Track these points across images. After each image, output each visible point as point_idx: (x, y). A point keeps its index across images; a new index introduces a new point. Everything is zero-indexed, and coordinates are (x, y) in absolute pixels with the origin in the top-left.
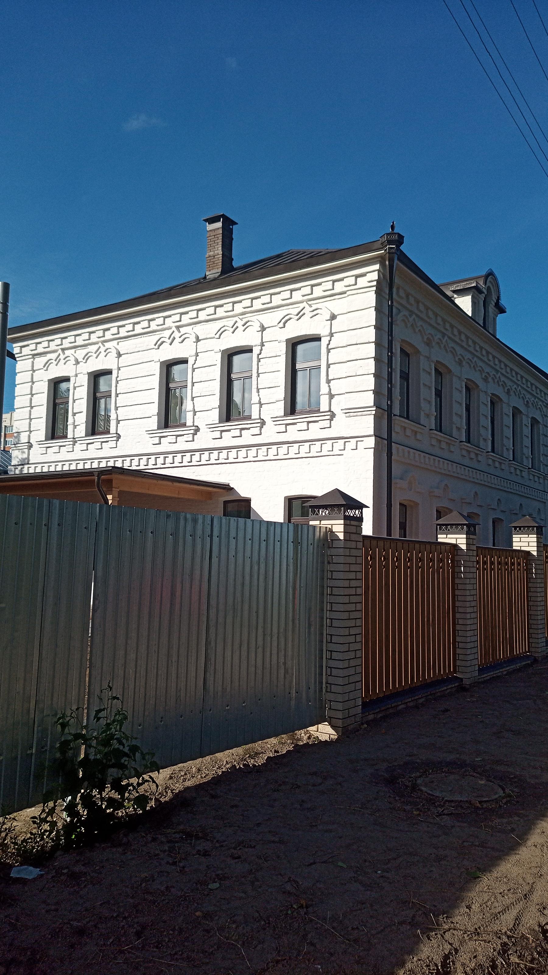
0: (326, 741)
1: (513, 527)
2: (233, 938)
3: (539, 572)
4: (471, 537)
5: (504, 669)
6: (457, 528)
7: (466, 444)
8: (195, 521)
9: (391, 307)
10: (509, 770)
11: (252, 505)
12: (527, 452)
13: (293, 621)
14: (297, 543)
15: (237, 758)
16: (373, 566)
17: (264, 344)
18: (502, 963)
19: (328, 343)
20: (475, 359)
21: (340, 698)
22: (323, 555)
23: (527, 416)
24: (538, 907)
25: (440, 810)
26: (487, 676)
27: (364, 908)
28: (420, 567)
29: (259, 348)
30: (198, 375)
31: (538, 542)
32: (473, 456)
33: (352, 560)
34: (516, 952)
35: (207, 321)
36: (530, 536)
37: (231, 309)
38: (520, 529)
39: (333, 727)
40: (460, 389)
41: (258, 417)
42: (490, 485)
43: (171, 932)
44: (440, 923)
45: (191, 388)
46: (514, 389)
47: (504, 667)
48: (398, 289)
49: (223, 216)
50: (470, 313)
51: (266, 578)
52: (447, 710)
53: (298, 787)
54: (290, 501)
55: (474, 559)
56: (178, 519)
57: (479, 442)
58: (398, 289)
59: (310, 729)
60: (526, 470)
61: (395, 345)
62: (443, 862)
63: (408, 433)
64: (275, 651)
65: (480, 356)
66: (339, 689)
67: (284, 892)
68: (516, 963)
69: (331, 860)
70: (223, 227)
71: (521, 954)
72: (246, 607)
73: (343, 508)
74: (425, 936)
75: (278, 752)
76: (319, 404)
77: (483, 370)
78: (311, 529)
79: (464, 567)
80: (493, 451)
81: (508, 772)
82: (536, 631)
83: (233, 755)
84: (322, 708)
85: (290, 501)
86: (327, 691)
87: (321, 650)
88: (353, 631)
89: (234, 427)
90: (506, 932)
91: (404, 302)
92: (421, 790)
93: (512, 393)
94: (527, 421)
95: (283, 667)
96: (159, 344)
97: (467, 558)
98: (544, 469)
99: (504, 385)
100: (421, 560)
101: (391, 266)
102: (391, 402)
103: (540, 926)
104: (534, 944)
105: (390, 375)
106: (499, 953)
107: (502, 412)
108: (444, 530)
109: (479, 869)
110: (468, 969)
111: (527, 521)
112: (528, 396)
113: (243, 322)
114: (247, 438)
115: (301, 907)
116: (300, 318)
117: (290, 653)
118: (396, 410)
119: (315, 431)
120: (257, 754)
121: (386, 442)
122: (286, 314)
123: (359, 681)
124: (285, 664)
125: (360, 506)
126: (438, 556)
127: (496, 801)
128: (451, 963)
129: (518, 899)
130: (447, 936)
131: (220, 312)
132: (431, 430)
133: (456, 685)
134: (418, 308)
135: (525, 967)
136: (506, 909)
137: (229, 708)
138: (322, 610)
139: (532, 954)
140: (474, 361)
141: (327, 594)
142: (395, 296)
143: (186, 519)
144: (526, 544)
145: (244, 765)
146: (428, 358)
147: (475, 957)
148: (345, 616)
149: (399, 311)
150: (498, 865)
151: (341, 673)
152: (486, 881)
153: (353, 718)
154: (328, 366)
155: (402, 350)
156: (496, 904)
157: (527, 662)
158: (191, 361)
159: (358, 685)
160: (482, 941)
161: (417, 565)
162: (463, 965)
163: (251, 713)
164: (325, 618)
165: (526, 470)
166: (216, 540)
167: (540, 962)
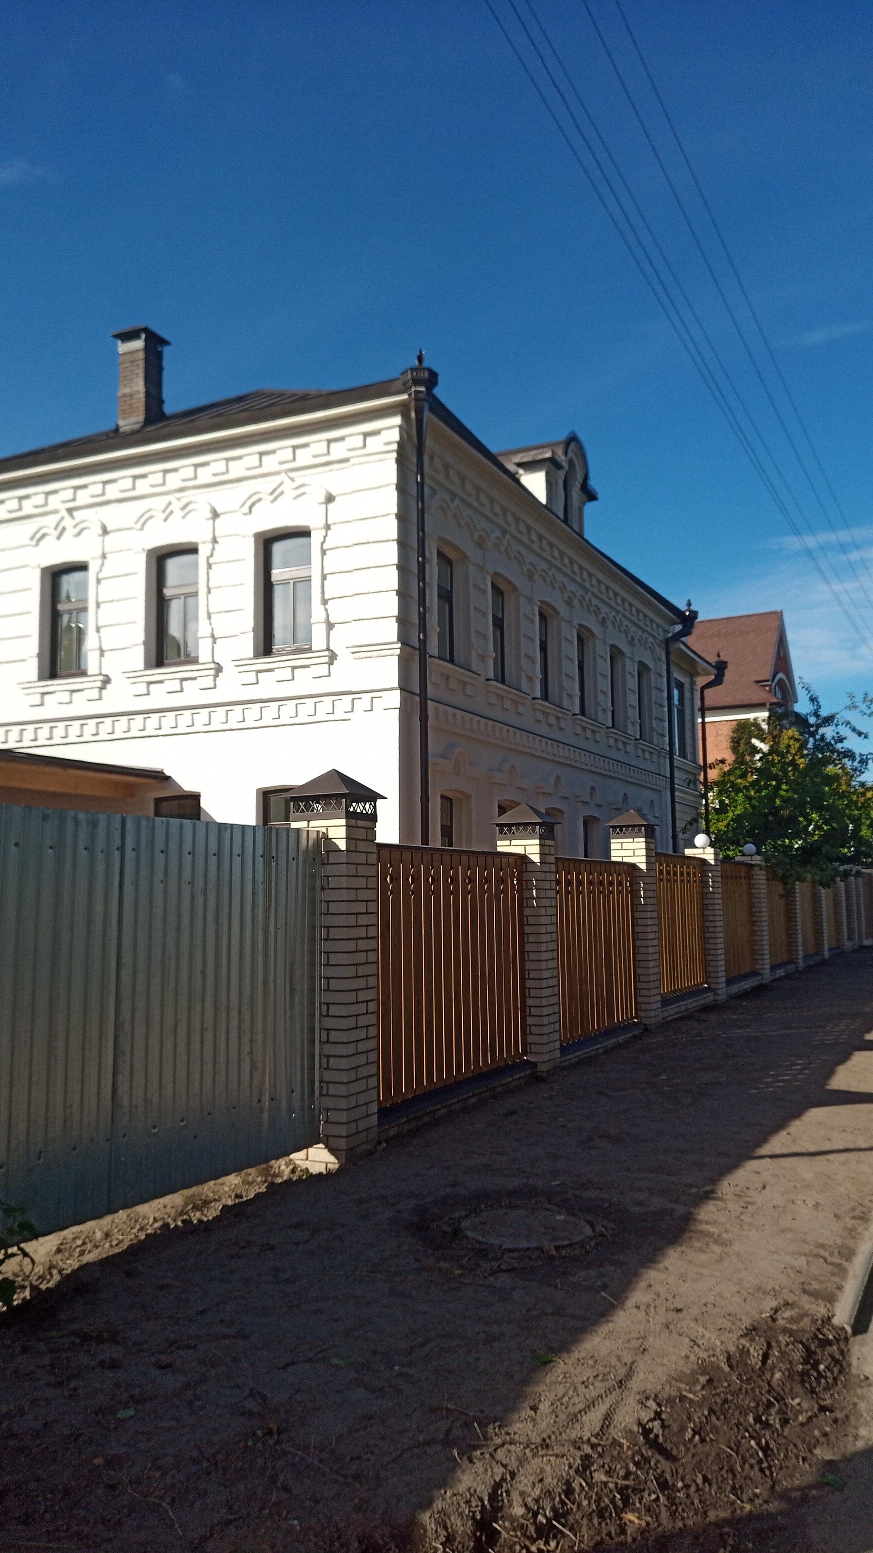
0: (321, 1174)
1: (611, 827)
2: (157, 1494)
3: (650, 894)
4: (547, 842)
5: (599, 1046)
6: (525, 829)
7: (541, 702)
8: (94, 824)
9: (421, 486)
10: (602, 1196)
11: (203, 804)
12: (633, 714)
13: (265, 983)
14: (269, 857)
15: (173, 1211)
16: (395, 892)
17: (218, 540)
18: (581, 1485)
19: (322, 540)
20: (553, 570)
21: (343, 1104)
22: (313, 876)
23: (632, 660)
24: (638, 1397)
25: (495, 1264)
26: (572, 1057)
27: (371, 1426)
28: (469, 892)
29: (210, 546)
30: (107, 591)
31: (647, 849)
32: (552, 720)
33: (361, 883)
34: (603, 1466)
35: (120, 501)
36: (636, 840)
37: (161, 481)
38: (621, 830)
39: (332, 1151)
40: (531, 616)
41: (211, 660)
42: (578, 765)
43: (50, 1496)
44: (489, 1436)
45: (94, 611)
46: (611, 618)
47: (600, 1043)
48: (431, 458)
49: (146, 330)
50: (543, 499)
51: (217, 916)
52: (513, 1112)
53: (272, 1248)
54: (266, 796)
55: (552, 877)
56: (62, 820)
57: (561, 699)
58: (431, 458)
59: (292, 1156)
60: (632, 742)
61: (429, 547)
62: (495, 1344)
63: (453, 684)
64: (234, 1035)
65: (560, 565)
66: (342, 1090)
67: (243, 1414)
68: (601, 1482)
69: (319, 1356)
70: (147, 349)
71: (610, 1468)
72: (184, 965)
73: (344, 800)
74: (465, 1458)
75: (241, 1197)
76: (309, 639)
77: (565, 588)
78: (292, 834)
79: (537, 889)
80: (583, 712)
81: (601, 1198)
82: (647, 986)
83: (165, 1207)
84: (314, 1122)
85: (266, 796)
86: (321, 1095)
87: (312, 1029)
88: (362, 996)
89: (170, 674)
90: (589, 1440)
91: (441, 478)
92: (466, 1237)
93: (609, 624)
94: (632, 668)
95: (248, 1059)
96: (39, 538)
97: (541, 876)
98: (658, 739)
99: (597, 612)
100: (471, 880)
101: (419, 420)
102: (425, 635)
103: (640, 1424)
104: (630, 1453)
105: (422, 593)
106: (577, 1471)
107: (595, 652)
108: (506, 833)
109: (552, 1350)
110: (530, 1499)
111: (631, 817)
112: (633, 629)
113: (182, 504)
114: (193, 694)
115: (270, 1433)
116: (275, 499)
117: (260, 1037)
118: (433, 648)
119: (304, 682)
120: (206, 1203)
121: (417, 699)
122: (253, 492)
123: (373, 1075)
124: (251, 1053)
125: (373, 797)
126: (497, 874)
127: (582, 1244)
128: (504, 1494)
129: (609, 1389)
130: (500, 1454)
131: (143, 487)
132: (487, 680)
133: (527, 1072)
134: (463, 488)
135: (616, 1487)
136: (591, 1405)
137: (156, 1130)
138: (312, 964)
139: (627, 1467)
140: (550, 574)
141: (321, 939)
142: (426, 468)
143: (76, 822)
144: (631, 853)
145: (183, 1221)
146: (481, 568)
147: (541, 1480)
148: (350, 972)
149: (434, 492)
150: (583, 1341)
151: (344, 1063)
152: (563, 1366)
153: (363, 1136)
154: (324, 577)
155: (440, 554)
156: (576, 1400)
157: (634, 1033)
158: (93, 568)
159: (372, 1082)
160: (552, 1455)
161: (464, 888)
162: (522, 1494)
163: (195, 1137)
164: (317, 977)
165: (632, 742)
166: (129, 854)
167: (638, 1477)
